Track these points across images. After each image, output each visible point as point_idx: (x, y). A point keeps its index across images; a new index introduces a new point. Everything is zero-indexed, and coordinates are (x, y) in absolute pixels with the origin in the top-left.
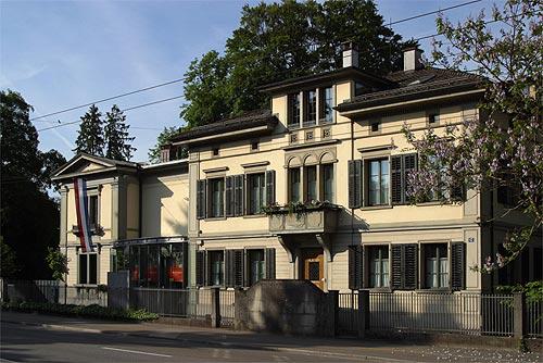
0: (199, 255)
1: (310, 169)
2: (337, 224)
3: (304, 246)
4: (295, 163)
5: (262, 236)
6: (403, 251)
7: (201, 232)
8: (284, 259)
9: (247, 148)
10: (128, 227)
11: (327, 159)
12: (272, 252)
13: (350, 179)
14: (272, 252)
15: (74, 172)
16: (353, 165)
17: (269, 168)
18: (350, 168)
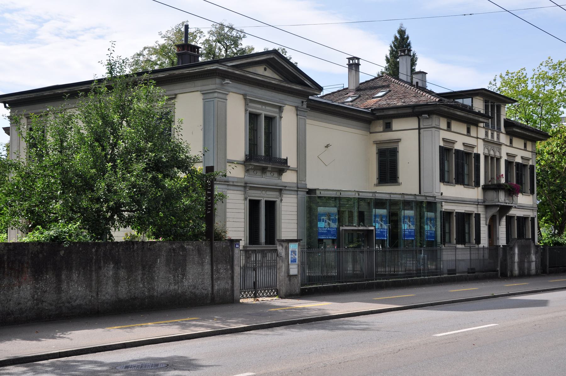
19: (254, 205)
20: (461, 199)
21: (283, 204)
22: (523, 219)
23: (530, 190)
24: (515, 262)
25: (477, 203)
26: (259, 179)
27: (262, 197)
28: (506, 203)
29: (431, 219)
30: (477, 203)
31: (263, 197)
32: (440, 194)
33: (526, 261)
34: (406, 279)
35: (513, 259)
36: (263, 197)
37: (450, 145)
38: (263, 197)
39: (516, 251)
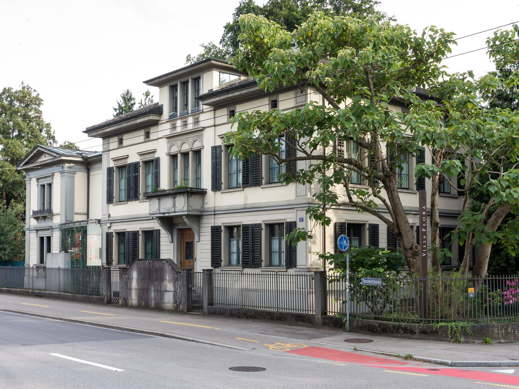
1: (185, 155)
2: (203, 206)
3: (181, 227)
4: (174, 150)
5: (289, 207)
7: (109, 216)
10: (76, 210)
11: (197, 146)
13: (212, 163)
16: (215, 149)
17: (156, 155)
18: (108, 172)
21: (54, 238)
25: (213, 213)
26: (43, 224)
31: (45, 234)
32: (107, 216)
33: (153, 289)
35: (129, 285)
39: (135, 275)
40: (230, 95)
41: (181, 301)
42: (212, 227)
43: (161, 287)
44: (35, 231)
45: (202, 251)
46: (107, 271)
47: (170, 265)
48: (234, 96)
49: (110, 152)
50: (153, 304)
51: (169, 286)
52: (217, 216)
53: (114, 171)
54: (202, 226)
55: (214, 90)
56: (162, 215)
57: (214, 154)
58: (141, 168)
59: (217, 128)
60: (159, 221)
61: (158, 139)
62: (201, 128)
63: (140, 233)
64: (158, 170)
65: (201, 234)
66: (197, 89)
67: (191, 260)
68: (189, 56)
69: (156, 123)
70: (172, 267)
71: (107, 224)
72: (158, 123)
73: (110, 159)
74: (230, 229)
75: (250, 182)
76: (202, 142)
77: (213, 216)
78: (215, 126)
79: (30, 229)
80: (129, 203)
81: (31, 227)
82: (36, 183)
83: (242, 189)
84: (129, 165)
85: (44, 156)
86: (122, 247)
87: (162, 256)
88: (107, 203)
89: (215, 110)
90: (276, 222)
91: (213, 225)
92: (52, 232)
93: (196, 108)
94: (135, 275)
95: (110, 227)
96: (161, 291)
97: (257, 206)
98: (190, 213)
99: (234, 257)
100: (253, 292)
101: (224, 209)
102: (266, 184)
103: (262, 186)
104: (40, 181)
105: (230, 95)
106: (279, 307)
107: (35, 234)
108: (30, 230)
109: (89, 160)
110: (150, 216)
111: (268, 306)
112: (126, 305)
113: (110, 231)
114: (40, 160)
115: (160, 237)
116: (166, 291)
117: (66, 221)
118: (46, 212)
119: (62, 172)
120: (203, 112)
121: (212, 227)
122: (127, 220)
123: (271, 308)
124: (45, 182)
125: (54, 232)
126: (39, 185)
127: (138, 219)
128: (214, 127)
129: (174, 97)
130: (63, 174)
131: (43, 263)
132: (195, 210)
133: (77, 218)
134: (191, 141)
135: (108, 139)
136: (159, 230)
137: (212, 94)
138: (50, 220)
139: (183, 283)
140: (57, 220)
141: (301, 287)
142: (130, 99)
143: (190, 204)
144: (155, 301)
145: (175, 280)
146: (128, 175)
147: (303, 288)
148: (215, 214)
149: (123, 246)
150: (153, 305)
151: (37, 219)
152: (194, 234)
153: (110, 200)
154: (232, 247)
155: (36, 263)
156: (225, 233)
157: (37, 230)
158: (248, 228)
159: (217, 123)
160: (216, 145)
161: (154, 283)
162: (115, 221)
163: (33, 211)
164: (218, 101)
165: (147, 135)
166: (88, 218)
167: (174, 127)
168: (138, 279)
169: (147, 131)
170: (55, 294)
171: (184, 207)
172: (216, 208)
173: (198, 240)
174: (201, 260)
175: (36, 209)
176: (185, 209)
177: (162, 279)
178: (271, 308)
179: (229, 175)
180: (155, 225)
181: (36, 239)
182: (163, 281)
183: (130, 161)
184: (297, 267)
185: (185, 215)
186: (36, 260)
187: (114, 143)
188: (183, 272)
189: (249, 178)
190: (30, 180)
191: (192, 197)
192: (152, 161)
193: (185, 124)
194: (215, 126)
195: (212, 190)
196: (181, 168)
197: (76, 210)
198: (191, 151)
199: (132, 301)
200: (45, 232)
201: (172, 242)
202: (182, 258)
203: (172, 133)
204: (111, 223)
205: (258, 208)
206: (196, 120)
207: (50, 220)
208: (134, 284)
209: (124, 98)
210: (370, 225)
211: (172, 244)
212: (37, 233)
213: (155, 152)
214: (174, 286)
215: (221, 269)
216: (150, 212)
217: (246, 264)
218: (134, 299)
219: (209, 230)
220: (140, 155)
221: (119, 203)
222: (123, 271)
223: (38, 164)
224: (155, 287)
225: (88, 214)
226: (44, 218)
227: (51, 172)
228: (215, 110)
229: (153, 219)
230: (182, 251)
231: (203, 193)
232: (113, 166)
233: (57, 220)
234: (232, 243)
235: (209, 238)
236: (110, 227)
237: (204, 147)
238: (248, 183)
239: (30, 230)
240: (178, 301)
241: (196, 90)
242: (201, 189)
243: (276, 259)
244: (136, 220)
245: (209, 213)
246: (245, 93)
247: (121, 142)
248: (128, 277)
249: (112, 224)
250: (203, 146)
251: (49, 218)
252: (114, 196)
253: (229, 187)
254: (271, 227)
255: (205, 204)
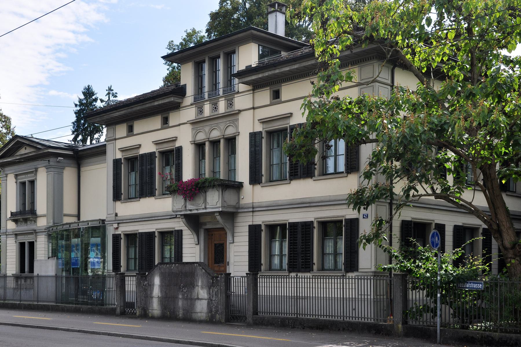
0: (116, 238)
1: (215, 143)
3: (208, 226)
4: (201, 137)
6: (299, 229)
7: (116, 215)
8: (189, 237)
9: (156, 122)
10: (65, 212)
11: (230, 132)
12: (179, 233)
14: (179, 233)
15: (9, 156)
16: (254, 137)
17: (177, 144)
18: (114, 165)
19: (22, 245)
20: (299, 201)
21: (38, 243)
22: (178, 232)
23: (156, 189)
24: (152, 297)
25: (251, 210)
26: (24, 227)
27: (25, 240)
28: (190, 210)
29: (97, 245)
30: (173, 217)
31: (26, 239)
32: (114, 215)
33: (180, 296)
34: (74, 305)
35: (149, 293)
36: (26, 240)
37: (132, 153)
38: (26, 240)
39: (157, 281)
40: (277, 71)
41: (218, 310)
42: (249, 226)
43: (191, 295)
44: (14, 236)
45: (236, 254)
46: (120, 277)
47: (203, 268)
48: (282, 73)
49: (117, 141)
50: (181, 314)
51: (202, 293)
52: (255, 214)
53: (122, 163)
54: (237, 224)
55: (253, 66)
56: (189, 212)
57: (254, 141)
58: (157, 159)
59: (256, 110)
60: (184, 220)
61: (179, 125)
62: (237, 112)
63: (156, 234)
64: (180, 161)
65: (235, 235)
66: (229, 65)
67: (221, 265)
68: (172, 41)
69: (177, 107)
70: (205, 271)
71: (114, 225)
72: (179, 107)
73: (117, 150)
74: (272, 228)
75: (299, 173)
76: (237, 127)
77: (251, 214)
78: (254, 108)
79: (7, 233)
80: (143, 200)
81: (8, 231)
82: (15, 180)
83: (289, 182)
84: (142, 156)
85: (24, 149)
86: (132, 251)
87: (185, 260)
88: (113, 200)
89: (253, 90)
90: (332, 219)
91: (251, 223)
92: (36, 236)
93: (214, 92)
94: (157, 281)
95: (117, 228)
96: (191, 299)
97: (308, 200)
98: (225, 210)
99: (276, 261)
100: (303, 300)
101: (264, 204)
102: (319, 175)
103: (314, 178)
104: (19, 177)
105: (277, 71)
106: (345, 315)
107: (14, 239)
108: (7, 235)
109: (80, 153)
110: (174, 214)
111: (331, 314)
112: (145, 315)
113: (117, 233)
114: (18, 153)
115: (182, 239)
116: (198, 299)
117: (54, 223)
118: (28, 213)
119: (47, 168)
120: (238, 92)
121: (249, 226)
122: (140, 220)
123: (329, 316)
124: (26, 179)
125: (38, 237)
126: (18, 182)
127: (154, 219)
128: (252, 110)
129: (199, 76)
130: (50, 170)
131: (24, 272)
132: (229, 206)
133: (66, 220)
134: (222, 126)
135: (114, 127)
136: (181, 231)
137: (249, 71)
138: (33, 222)
139: (220, 289)
140: (42, 223)
141: (363, 293)
142: (93, 94)
143: (225, 199)
144: (183, 310)
145: (210, 287)
146: (140, 168)
147: (364, 295)
148: (253, 212)
149: (133, 249)
150: (180, 315)
151: (16, 221)
152: (226, 234)
153: (117, 196)
154: (273, 249)
155: (14, 272)
156: (266, 233)
157: (16, 235)
158: (297, 226)
159: (256, 105)
160: (255, 131)
161: (183, 290)
162: (124, 221)
163: (12, 213)
164: (260, 78)
165: (165, 121)
166: (79, 219)
167: (201, 111)
168: (161, 286)
169: (165, 116)
170: (52, 305)
171: (218, 203)
172: (254, 204)
173: (232, 242)
174: (236, 264)
175: (14, 210)
176: (219, 205)
177: (192, 285)
178: (329, 316)
179: (270, 166)
180: (179, 225)
181: (15, 244)
182: (194, 287)
183: (142, 151)
184: (360, 270)
185: (219, 212)
186: (15, 269)
187: (121, 130)
188: (221, 276)
189: (297, 169)
190: (6, 177)
191: (227, 191)
192: (171, 151)
193: (215, 107)
194: (254, 108)
195: (250, 184)
196: (210, 158)
197: (65, 212)
198: (208, 141)
199: (154, 311)
200: (26, 236)
201: (198, 244)
202: (210, 262)
203: (197, 118)
204: (118, 223)
205: (309, 203)
206: (229, 102)
207: (33, 222)
208: (156, 291)
209: (84, 93)
210: (436, 224)
211: (198, 247)
212: (16, 238)
213: (175, 140)
214: (209, 293)
215: (261, 274)
216: (173, 209)
217: (294, 267)
218: (155, 307)
219: (247, 229)
220: (156, 144)
221: (129, 200)
222: (141, 277)
223: (18, 158)
224: (183, 295)
225: (78, 216)
226: (26, 220)
227: (34, 167)
228: (253, 90)
229: (176, 217)
230: (210, 255)
231: (239, 186)
232: (154, 150)
233: (42, 223)
234: (273, 244)
235: (247, 239)
236: (117, 228)
237: (240, 134)
238: (297, 175)
239: (7, 235)
240: (213, 310)
241: (228, 67)
242: (235, 182)
243: (329, 262)
244: (151, 219)
245: (246, 210)
246: (296, 69)
247: (130, 129)
248: (148, 284)
249: (120, 225)
250: (239, 133)
251: (31, 220)
252: (122, 192)
253: (271, 180)
254: (324, 225)
255: (241, 199)
